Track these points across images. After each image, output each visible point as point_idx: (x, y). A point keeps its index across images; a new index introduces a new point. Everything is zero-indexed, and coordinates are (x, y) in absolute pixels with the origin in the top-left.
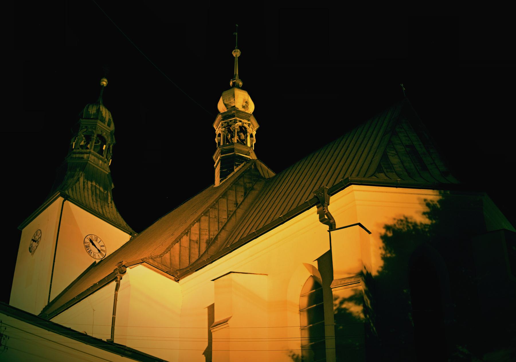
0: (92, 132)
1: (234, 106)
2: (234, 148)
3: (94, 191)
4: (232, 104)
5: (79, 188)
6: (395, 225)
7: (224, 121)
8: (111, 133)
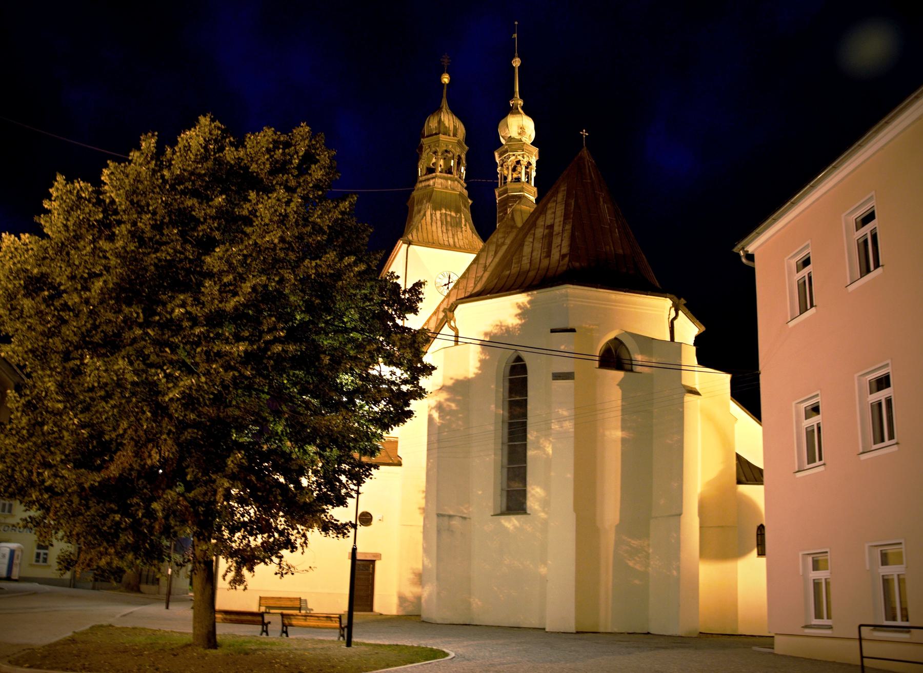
3: (444, 220)
8: (459, 142)
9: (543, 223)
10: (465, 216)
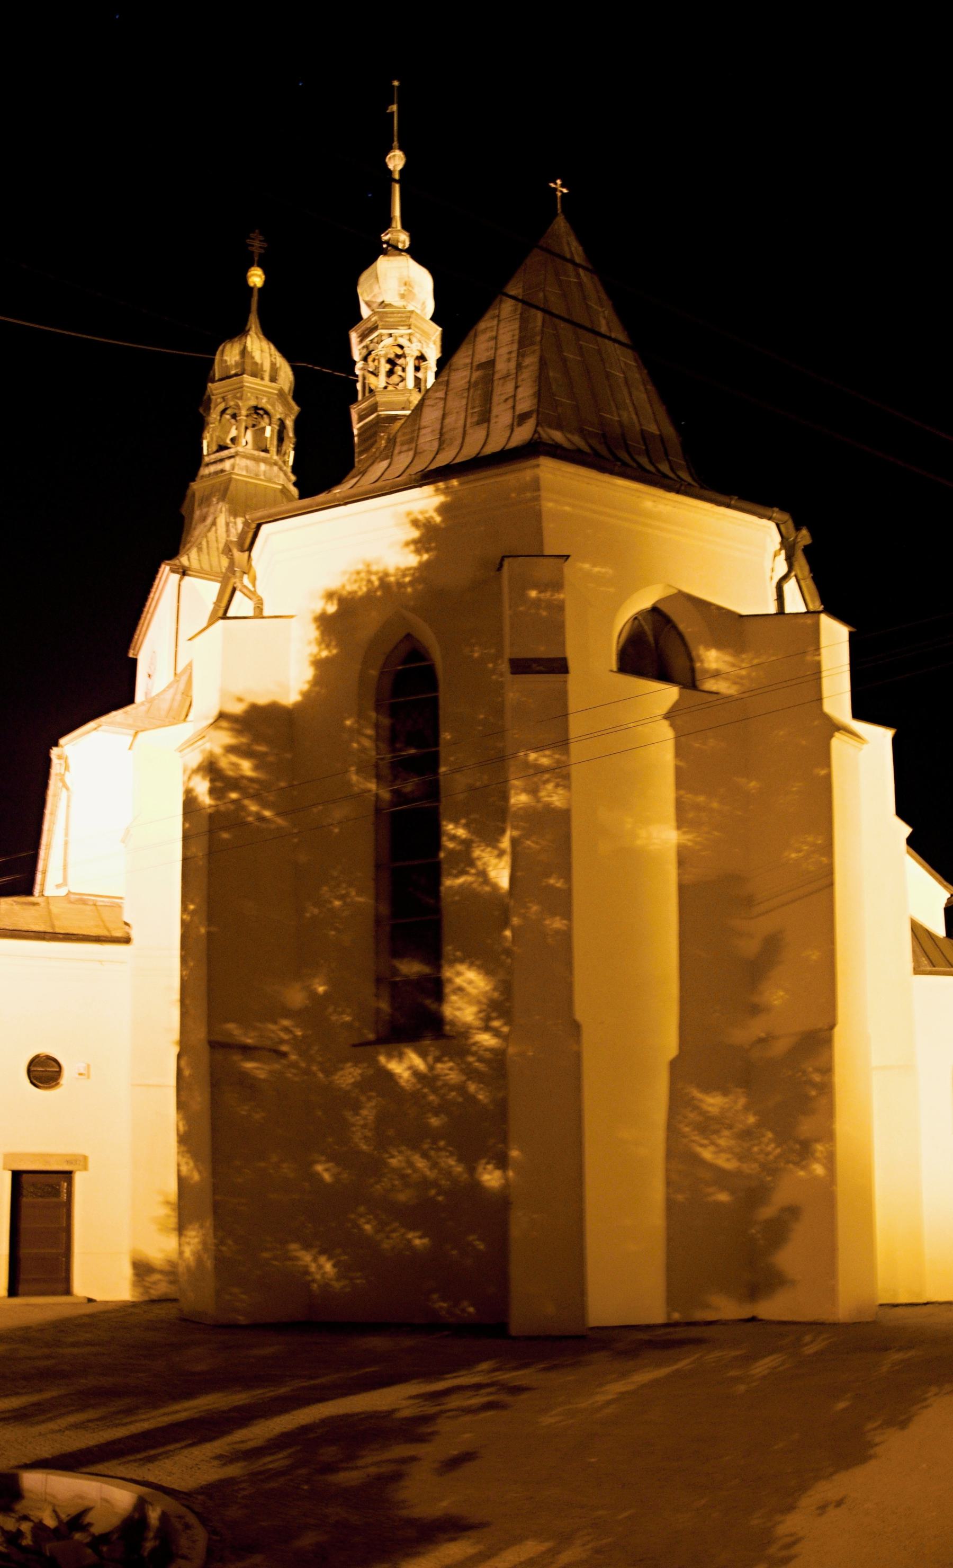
0: (238, 406)
1: (383, 302)
6: (344, 586)
8: (281, 393)
9: (468, 361)
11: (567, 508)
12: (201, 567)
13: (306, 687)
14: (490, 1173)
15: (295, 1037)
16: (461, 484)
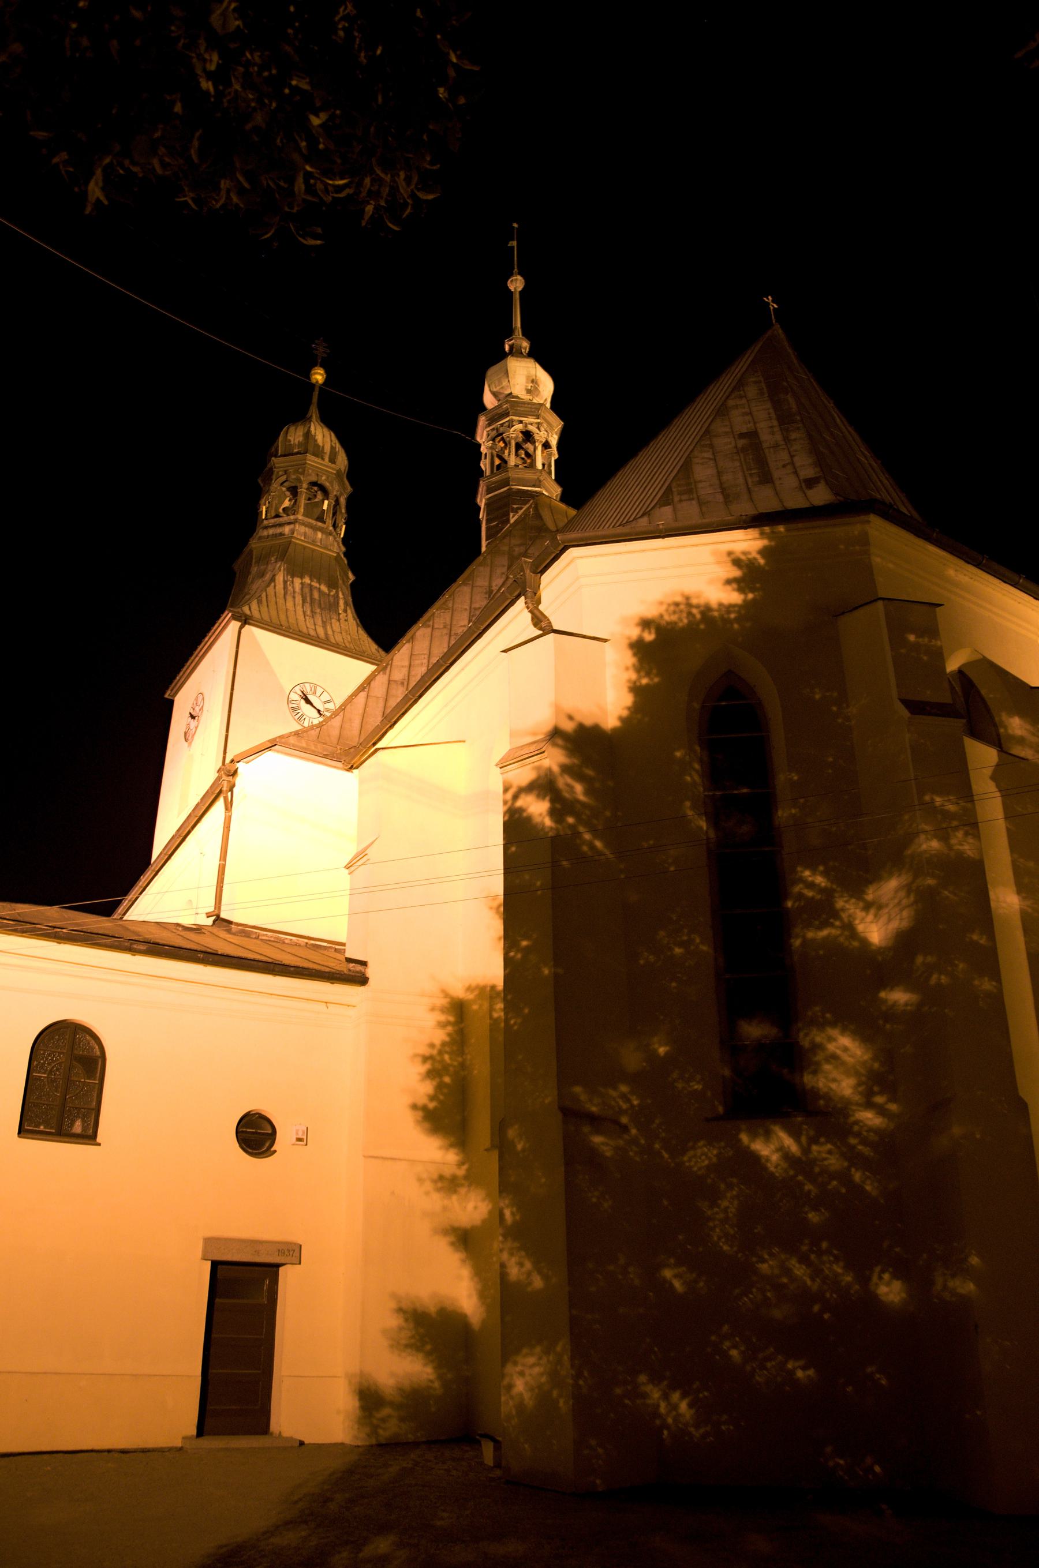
0: (299, 480)
1: (511, 394)
2: (509, 478)
3: (308, 595)
4: (506, 390)
5: (274, 594)
6: (661, 616)
7: (491, 428)
8: (339, 473)
10: (343, 598)
11: (891, 566)
12: (262, 618)
13: (625, 713)
14: (888, 1284)
15: (632, 1106)
16: (787, 530)
